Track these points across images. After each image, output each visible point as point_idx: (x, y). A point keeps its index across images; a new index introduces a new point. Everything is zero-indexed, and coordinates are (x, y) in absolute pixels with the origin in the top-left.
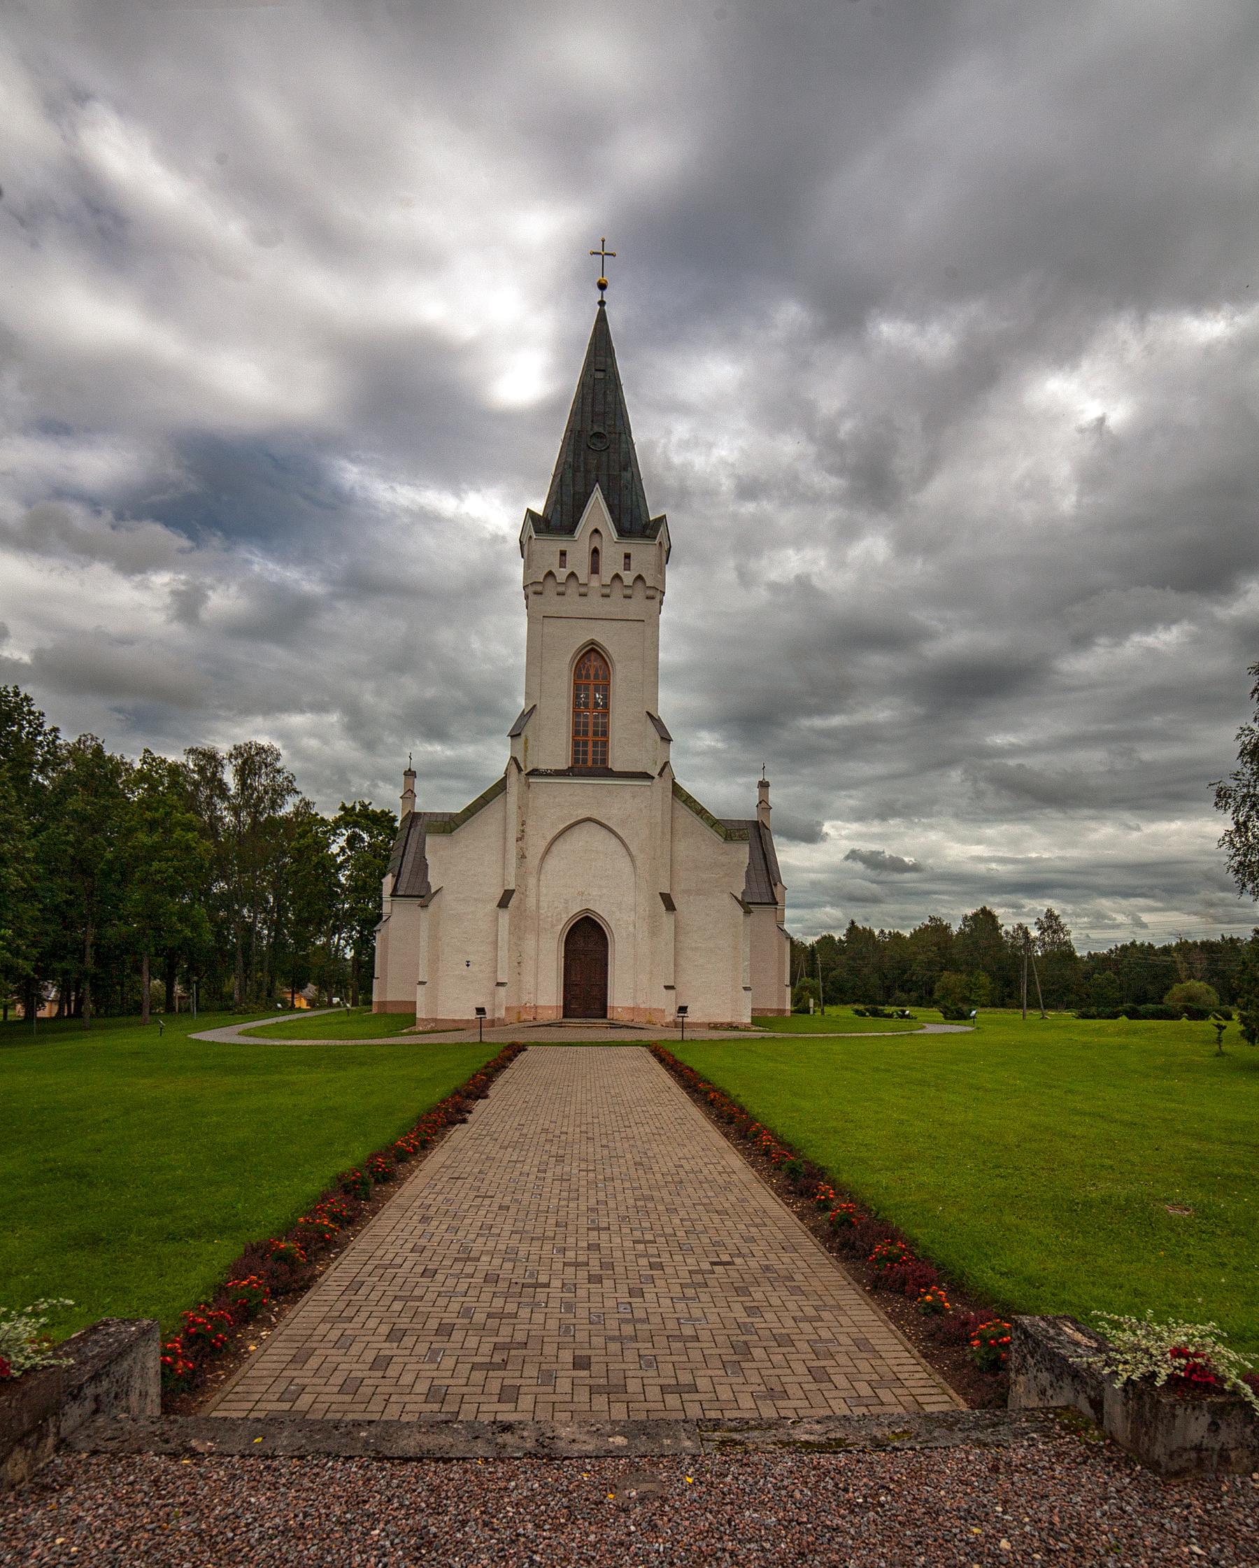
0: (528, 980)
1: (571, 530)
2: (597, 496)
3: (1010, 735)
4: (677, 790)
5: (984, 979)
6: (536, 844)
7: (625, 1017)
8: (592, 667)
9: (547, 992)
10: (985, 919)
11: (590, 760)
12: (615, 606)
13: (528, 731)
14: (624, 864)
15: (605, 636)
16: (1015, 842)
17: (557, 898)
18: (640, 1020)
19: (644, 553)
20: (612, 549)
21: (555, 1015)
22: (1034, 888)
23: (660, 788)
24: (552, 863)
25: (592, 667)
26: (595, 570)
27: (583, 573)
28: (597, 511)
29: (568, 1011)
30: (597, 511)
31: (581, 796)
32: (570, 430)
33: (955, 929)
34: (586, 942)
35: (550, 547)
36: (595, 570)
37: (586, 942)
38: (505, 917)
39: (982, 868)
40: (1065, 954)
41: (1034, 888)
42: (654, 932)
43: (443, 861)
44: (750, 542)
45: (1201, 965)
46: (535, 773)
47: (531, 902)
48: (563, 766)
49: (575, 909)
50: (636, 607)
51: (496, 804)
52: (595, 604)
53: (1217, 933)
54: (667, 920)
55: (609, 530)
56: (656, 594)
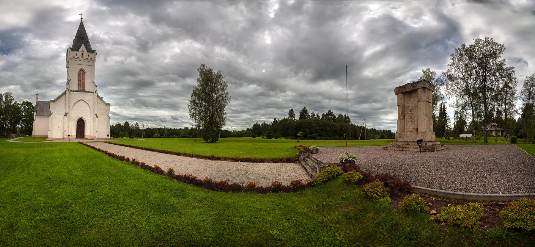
0: (70, 130)
1: (78, 50)
2: (83, 46)
3: (144, 94)
4: (98, 96)
5: (127, 133)
6: (72, 104)
7: (88, 138)
8: (82, 72)
9: (74, 133)
10: (127, 123)
11: (81, 88)
12: (86, 63)
13: (70, 83)
14: (88, 108)
15: (84, 68)
16: (134, 112)
17: (75, 116)
18: (91, 138)
19: (92, 55)
20: (86, 54)
21: (75, 137)
22: (134, 119)
23: (95, 95)
24: (74, 108)
25: (82, 72)
26: (82, 57)
27: (80, 57)
28: (83, 47)
29: (77, 136)
30: (83, 47)
31: (80, 95)
32: (78, 30)
33: (517, 121)
34: (81, 124)
35: (73, 53)
36: (82, 57)
37: (81, 124)
38: (66, 118)
39: (129, 115)
40: (138, 129)
41: (134, 119)
42: (94, 121)
43: (53, 108)
44: (108, 54)
45: (158, 131)
46: (71, 91)
47: (71, 115)
48: (77, 90)
49: (79, 117)
50: (90, 63)
51: (64, 97)
52: (82, 62)
53: (159, 127)
54: (97, 119)
55: (85, 51)
56: (94, 61)
